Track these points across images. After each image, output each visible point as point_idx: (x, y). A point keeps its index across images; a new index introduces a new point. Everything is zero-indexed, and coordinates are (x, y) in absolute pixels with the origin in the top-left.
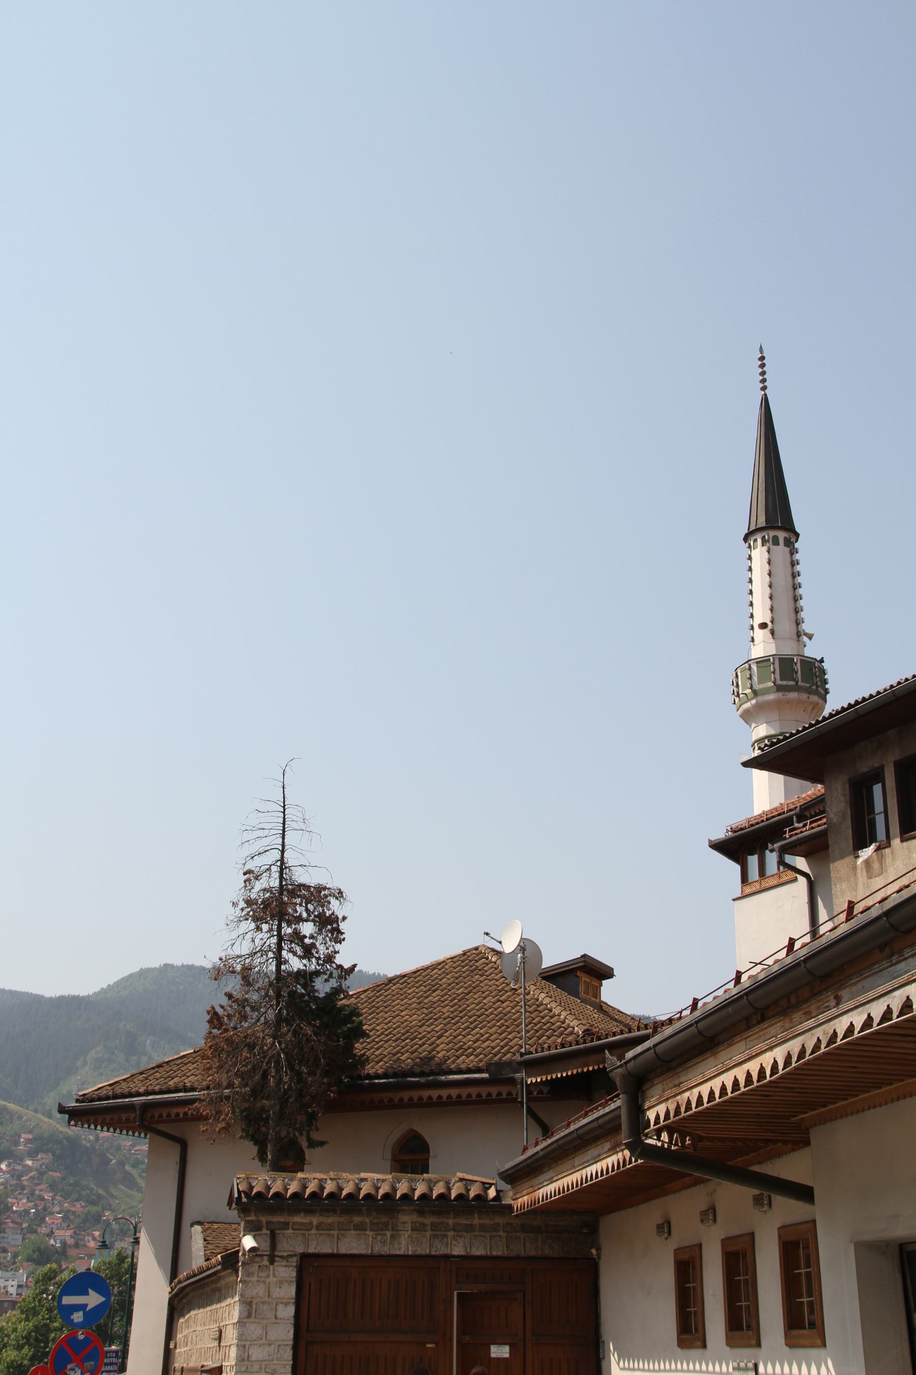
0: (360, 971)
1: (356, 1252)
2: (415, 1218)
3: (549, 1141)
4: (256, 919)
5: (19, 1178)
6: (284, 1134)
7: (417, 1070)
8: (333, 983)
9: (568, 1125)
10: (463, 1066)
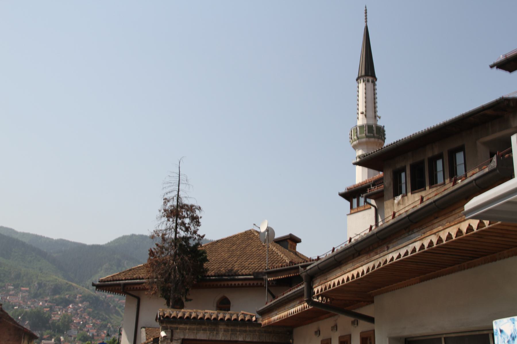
0: (206, 239)
1: (203, 338)
2: (225, 327)
3: (276, 300)
4: (167, 217)
5: (77, 310)
6: (176, 296)
7: (227, 274)
8: (196, 241)
9: (284, 294)
10: (244, 273)
